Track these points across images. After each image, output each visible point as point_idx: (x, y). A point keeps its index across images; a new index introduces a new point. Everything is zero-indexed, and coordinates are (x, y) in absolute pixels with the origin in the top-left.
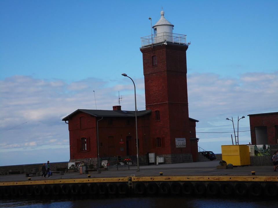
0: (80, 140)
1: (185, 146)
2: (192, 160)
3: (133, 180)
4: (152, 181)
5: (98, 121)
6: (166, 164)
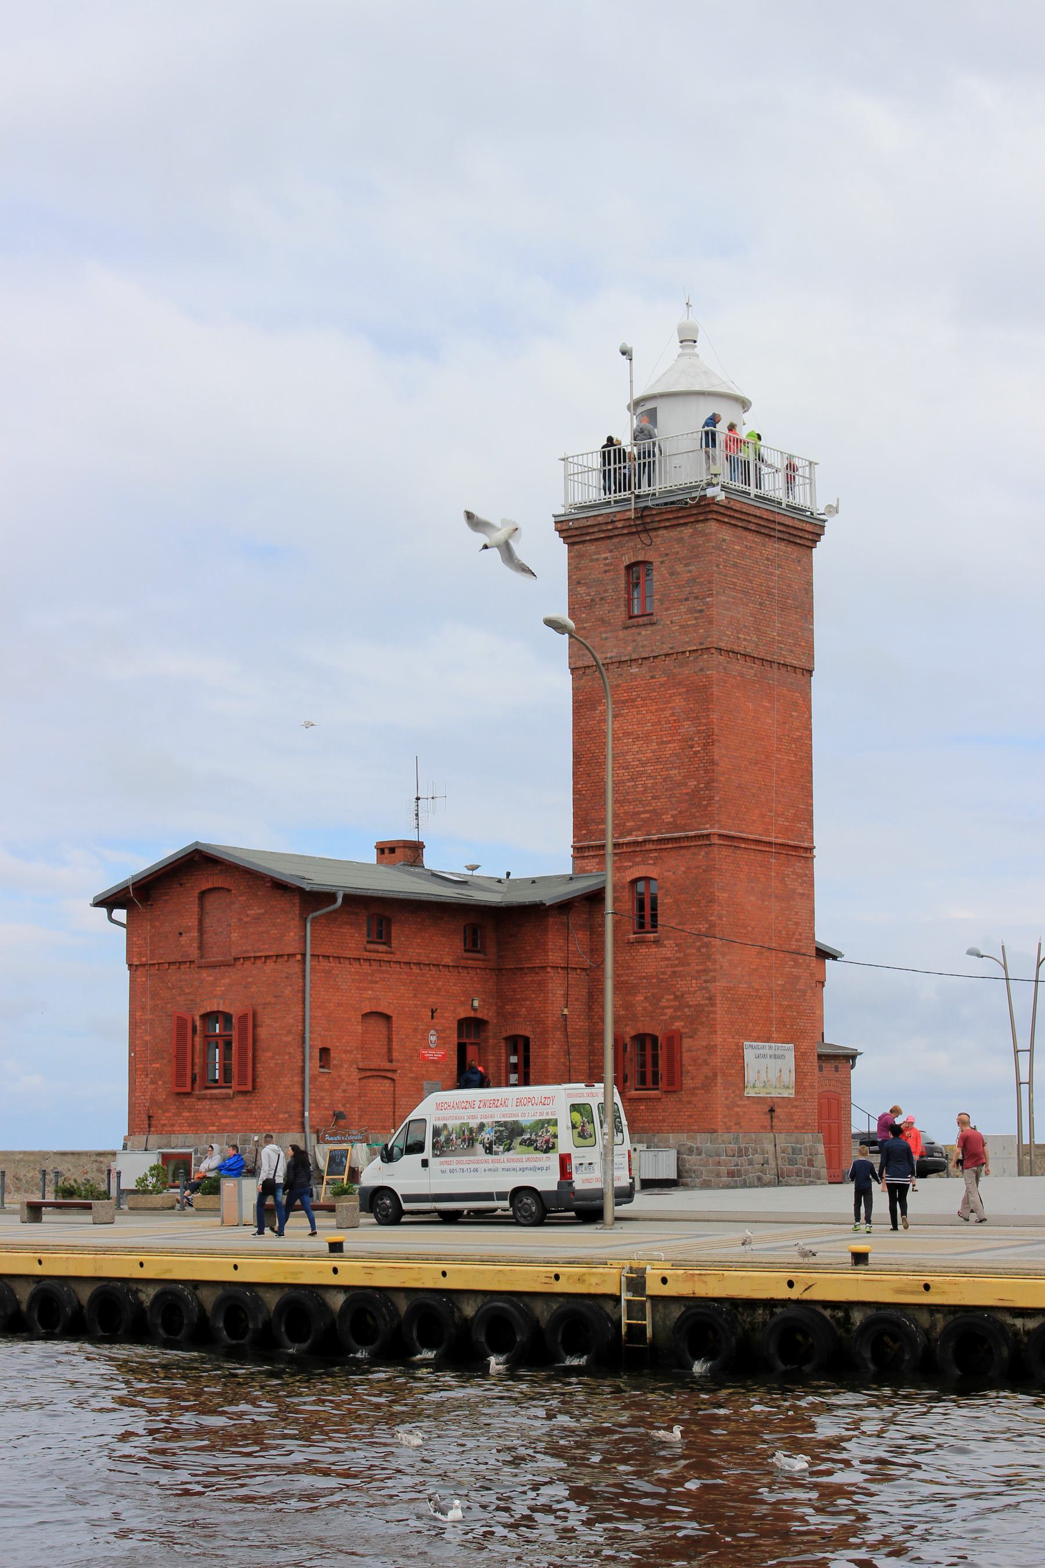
0: (198, 1023)
1: (788, 1087)
2: (824, 1172)
3: (654, 1288)
4: (798, 1302)
5: (311, 916)
6: (685, 1185)
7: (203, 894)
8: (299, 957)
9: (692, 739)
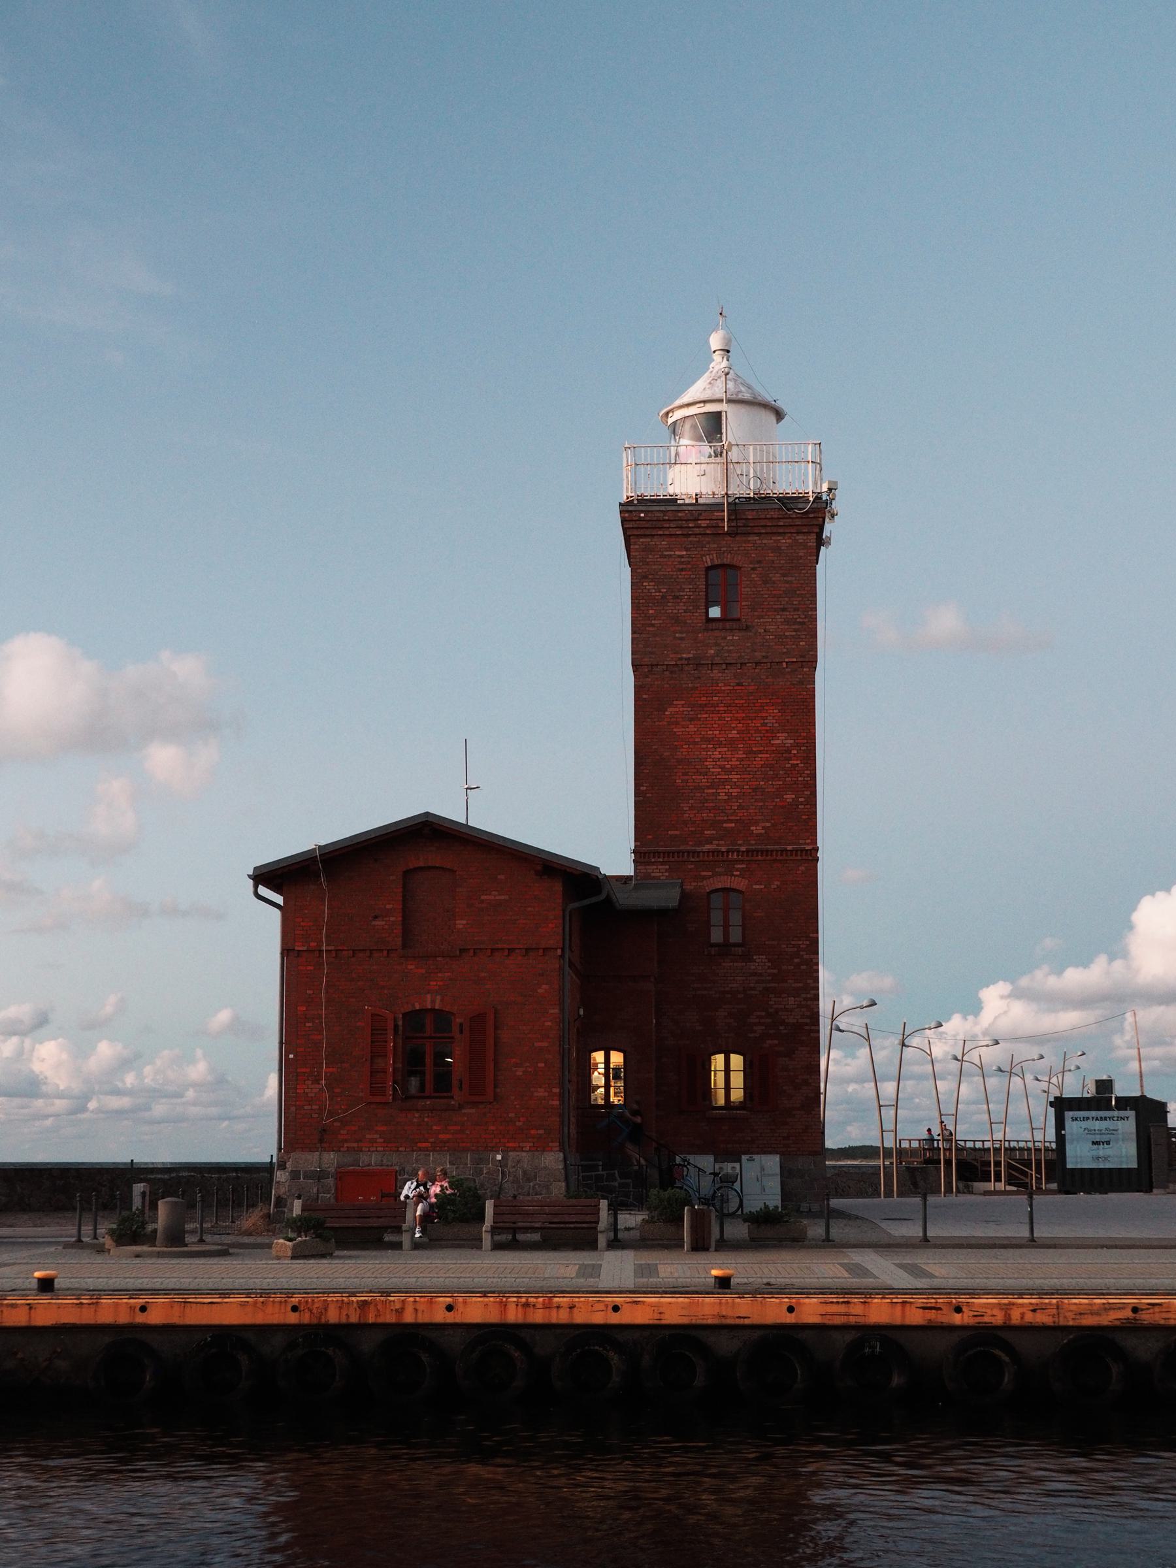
7: (407, 874)
8: (559, 952)
9: (788, 751)
